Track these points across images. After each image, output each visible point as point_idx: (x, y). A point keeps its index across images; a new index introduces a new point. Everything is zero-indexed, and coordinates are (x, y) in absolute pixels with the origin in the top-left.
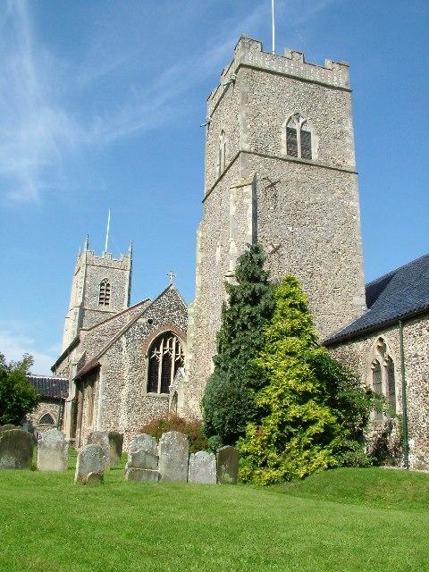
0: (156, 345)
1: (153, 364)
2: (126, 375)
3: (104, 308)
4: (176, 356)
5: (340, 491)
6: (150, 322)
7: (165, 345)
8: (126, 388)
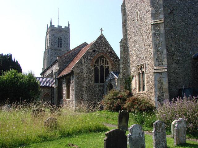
0: (97, 62)
1: (96, 69)
2: (85, 76)
3: (60, 48)
4: (106, 67)
5: (96, 81)
6: (94, 51)
7: (101, 62)
8: (85, 81)
